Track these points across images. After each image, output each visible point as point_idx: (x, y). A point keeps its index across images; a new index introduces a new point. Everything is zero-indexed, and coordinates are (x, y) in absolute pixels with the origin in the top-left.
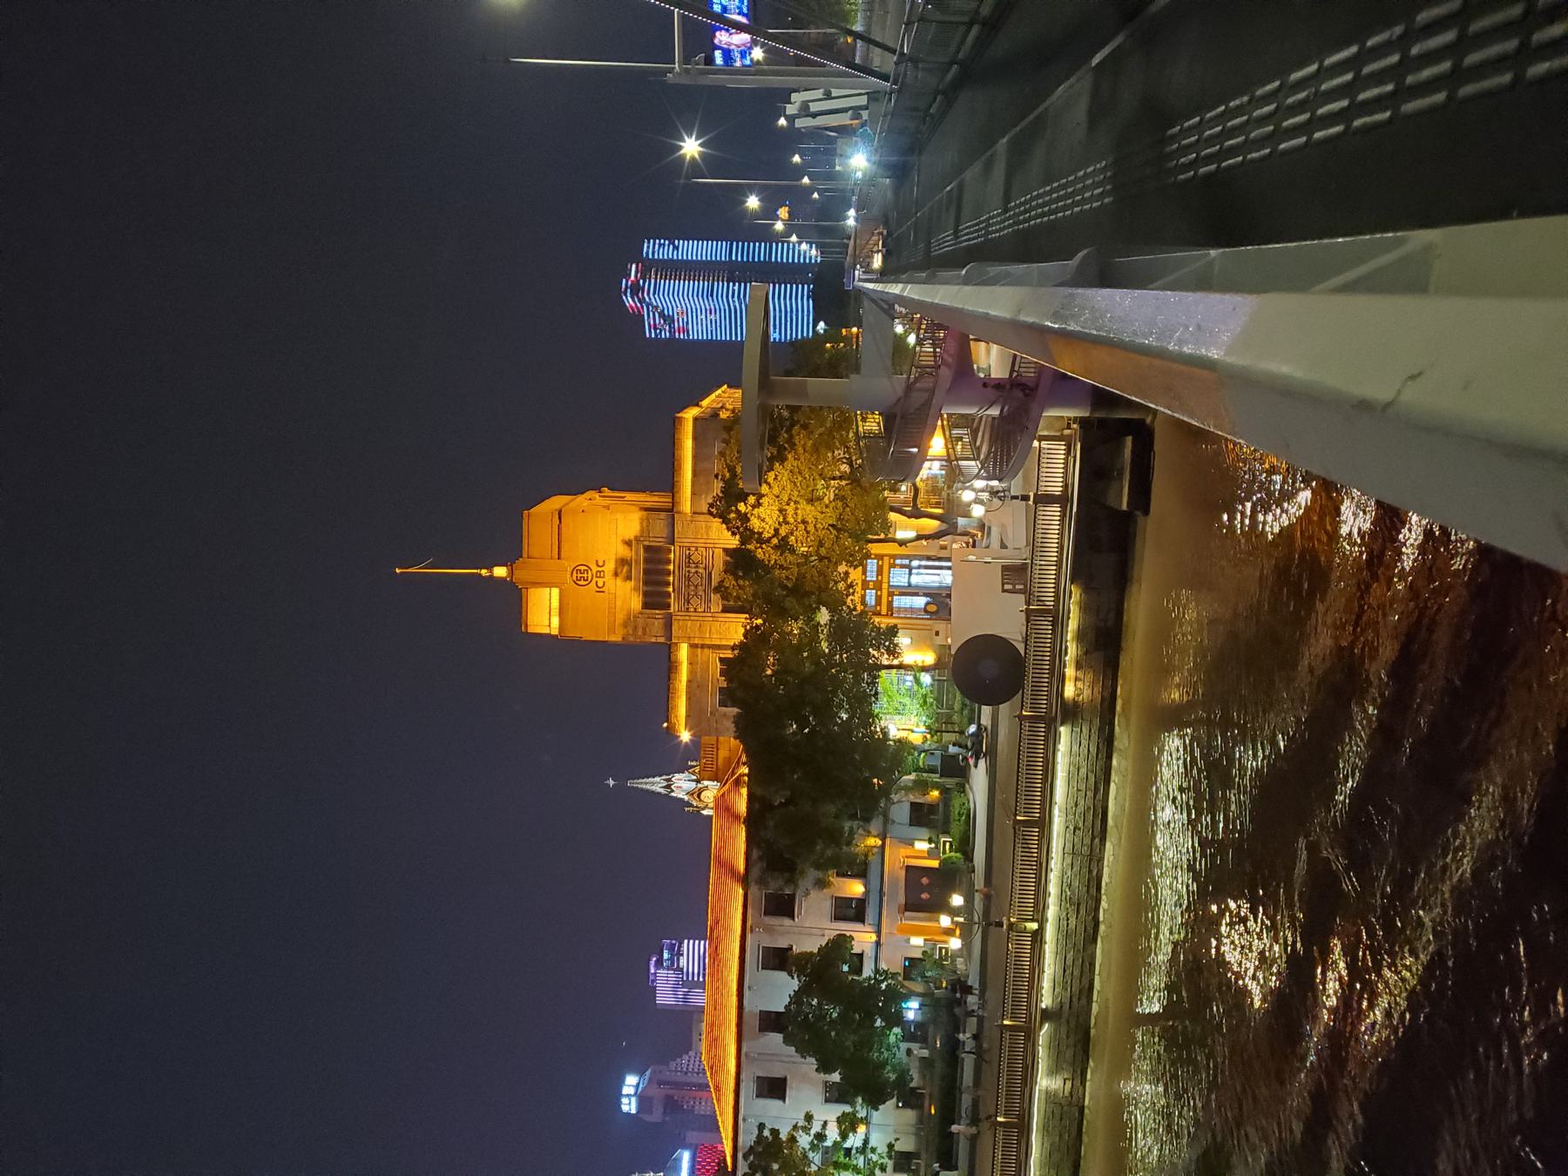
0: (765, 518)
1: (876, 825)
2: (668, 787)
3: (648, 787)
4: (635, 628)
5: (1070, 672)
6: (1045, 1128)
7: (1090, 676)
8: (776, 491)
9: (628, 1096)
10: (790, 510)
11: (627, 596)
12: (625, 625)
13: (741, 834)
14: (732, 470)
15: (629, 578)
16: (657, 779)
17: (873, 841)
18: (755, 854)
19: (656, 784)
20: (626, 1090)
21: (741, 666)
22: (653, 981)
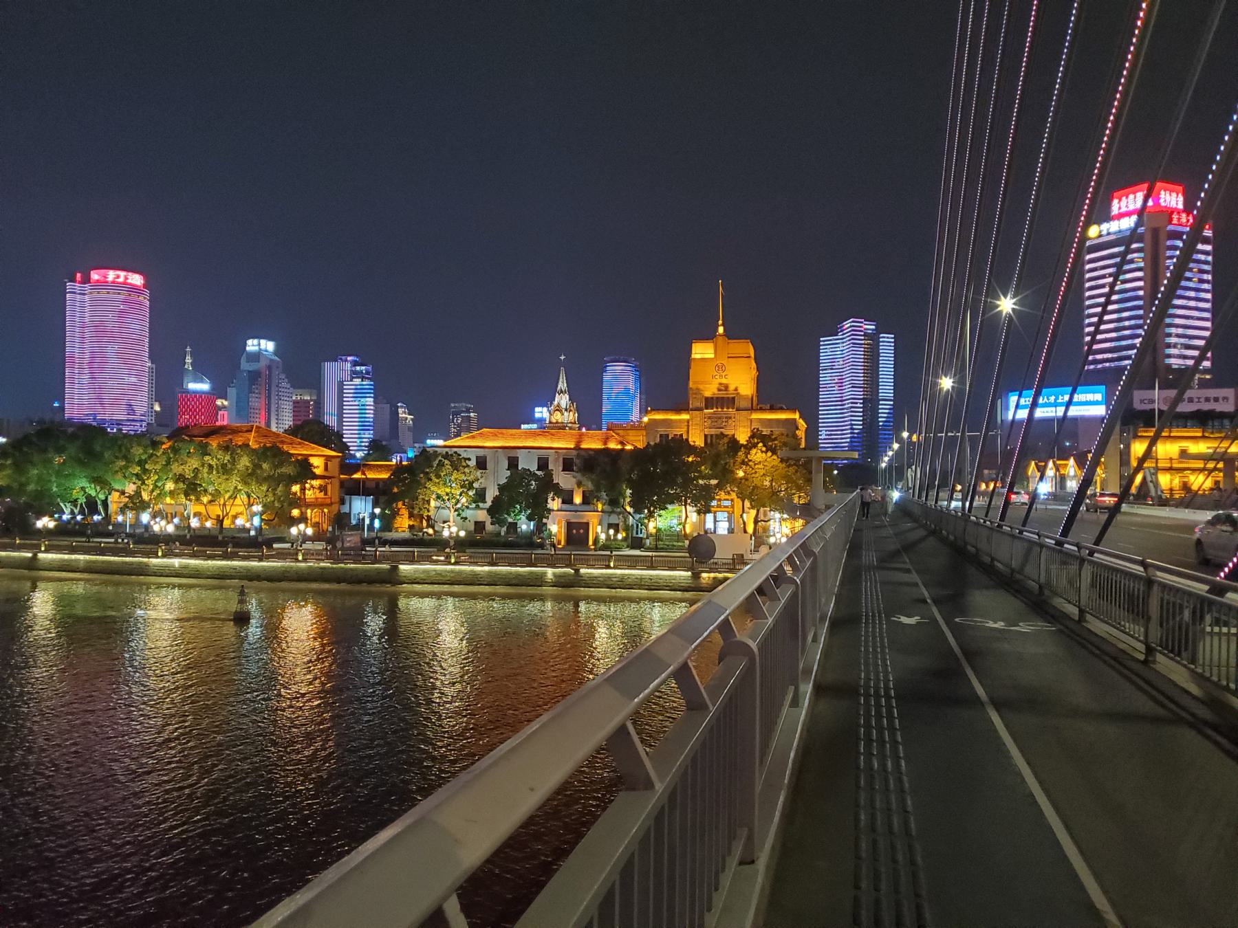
0: (757, 455)
1: (607, 508)
2: (562, 392)
3: (561, 380)
4: (696, 394)
5: (712, 575)
6: (531, 573)
7: (710, 582)
8: (768, 460)
9: (259, 345)
10: (761, 466)
11: (710, 391)
12: (697, 389)
13: (599, 446)
14: (775, 439)
15: (719, 390)
16: (565, 385)
17: (600, 507)
18: (591, 453)
19: (562, 385)
20: (263, 342)
21: (680, 445)
22: (341, 359)
